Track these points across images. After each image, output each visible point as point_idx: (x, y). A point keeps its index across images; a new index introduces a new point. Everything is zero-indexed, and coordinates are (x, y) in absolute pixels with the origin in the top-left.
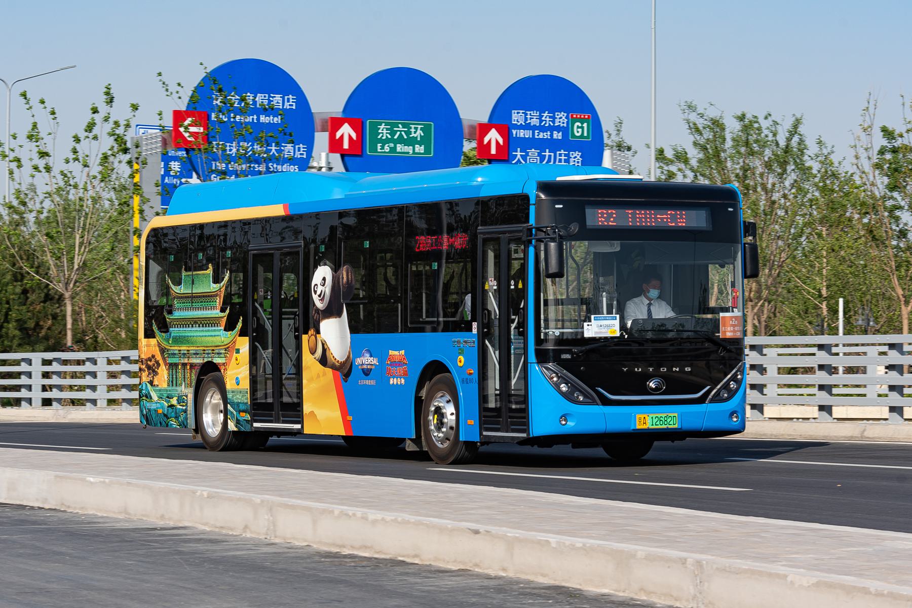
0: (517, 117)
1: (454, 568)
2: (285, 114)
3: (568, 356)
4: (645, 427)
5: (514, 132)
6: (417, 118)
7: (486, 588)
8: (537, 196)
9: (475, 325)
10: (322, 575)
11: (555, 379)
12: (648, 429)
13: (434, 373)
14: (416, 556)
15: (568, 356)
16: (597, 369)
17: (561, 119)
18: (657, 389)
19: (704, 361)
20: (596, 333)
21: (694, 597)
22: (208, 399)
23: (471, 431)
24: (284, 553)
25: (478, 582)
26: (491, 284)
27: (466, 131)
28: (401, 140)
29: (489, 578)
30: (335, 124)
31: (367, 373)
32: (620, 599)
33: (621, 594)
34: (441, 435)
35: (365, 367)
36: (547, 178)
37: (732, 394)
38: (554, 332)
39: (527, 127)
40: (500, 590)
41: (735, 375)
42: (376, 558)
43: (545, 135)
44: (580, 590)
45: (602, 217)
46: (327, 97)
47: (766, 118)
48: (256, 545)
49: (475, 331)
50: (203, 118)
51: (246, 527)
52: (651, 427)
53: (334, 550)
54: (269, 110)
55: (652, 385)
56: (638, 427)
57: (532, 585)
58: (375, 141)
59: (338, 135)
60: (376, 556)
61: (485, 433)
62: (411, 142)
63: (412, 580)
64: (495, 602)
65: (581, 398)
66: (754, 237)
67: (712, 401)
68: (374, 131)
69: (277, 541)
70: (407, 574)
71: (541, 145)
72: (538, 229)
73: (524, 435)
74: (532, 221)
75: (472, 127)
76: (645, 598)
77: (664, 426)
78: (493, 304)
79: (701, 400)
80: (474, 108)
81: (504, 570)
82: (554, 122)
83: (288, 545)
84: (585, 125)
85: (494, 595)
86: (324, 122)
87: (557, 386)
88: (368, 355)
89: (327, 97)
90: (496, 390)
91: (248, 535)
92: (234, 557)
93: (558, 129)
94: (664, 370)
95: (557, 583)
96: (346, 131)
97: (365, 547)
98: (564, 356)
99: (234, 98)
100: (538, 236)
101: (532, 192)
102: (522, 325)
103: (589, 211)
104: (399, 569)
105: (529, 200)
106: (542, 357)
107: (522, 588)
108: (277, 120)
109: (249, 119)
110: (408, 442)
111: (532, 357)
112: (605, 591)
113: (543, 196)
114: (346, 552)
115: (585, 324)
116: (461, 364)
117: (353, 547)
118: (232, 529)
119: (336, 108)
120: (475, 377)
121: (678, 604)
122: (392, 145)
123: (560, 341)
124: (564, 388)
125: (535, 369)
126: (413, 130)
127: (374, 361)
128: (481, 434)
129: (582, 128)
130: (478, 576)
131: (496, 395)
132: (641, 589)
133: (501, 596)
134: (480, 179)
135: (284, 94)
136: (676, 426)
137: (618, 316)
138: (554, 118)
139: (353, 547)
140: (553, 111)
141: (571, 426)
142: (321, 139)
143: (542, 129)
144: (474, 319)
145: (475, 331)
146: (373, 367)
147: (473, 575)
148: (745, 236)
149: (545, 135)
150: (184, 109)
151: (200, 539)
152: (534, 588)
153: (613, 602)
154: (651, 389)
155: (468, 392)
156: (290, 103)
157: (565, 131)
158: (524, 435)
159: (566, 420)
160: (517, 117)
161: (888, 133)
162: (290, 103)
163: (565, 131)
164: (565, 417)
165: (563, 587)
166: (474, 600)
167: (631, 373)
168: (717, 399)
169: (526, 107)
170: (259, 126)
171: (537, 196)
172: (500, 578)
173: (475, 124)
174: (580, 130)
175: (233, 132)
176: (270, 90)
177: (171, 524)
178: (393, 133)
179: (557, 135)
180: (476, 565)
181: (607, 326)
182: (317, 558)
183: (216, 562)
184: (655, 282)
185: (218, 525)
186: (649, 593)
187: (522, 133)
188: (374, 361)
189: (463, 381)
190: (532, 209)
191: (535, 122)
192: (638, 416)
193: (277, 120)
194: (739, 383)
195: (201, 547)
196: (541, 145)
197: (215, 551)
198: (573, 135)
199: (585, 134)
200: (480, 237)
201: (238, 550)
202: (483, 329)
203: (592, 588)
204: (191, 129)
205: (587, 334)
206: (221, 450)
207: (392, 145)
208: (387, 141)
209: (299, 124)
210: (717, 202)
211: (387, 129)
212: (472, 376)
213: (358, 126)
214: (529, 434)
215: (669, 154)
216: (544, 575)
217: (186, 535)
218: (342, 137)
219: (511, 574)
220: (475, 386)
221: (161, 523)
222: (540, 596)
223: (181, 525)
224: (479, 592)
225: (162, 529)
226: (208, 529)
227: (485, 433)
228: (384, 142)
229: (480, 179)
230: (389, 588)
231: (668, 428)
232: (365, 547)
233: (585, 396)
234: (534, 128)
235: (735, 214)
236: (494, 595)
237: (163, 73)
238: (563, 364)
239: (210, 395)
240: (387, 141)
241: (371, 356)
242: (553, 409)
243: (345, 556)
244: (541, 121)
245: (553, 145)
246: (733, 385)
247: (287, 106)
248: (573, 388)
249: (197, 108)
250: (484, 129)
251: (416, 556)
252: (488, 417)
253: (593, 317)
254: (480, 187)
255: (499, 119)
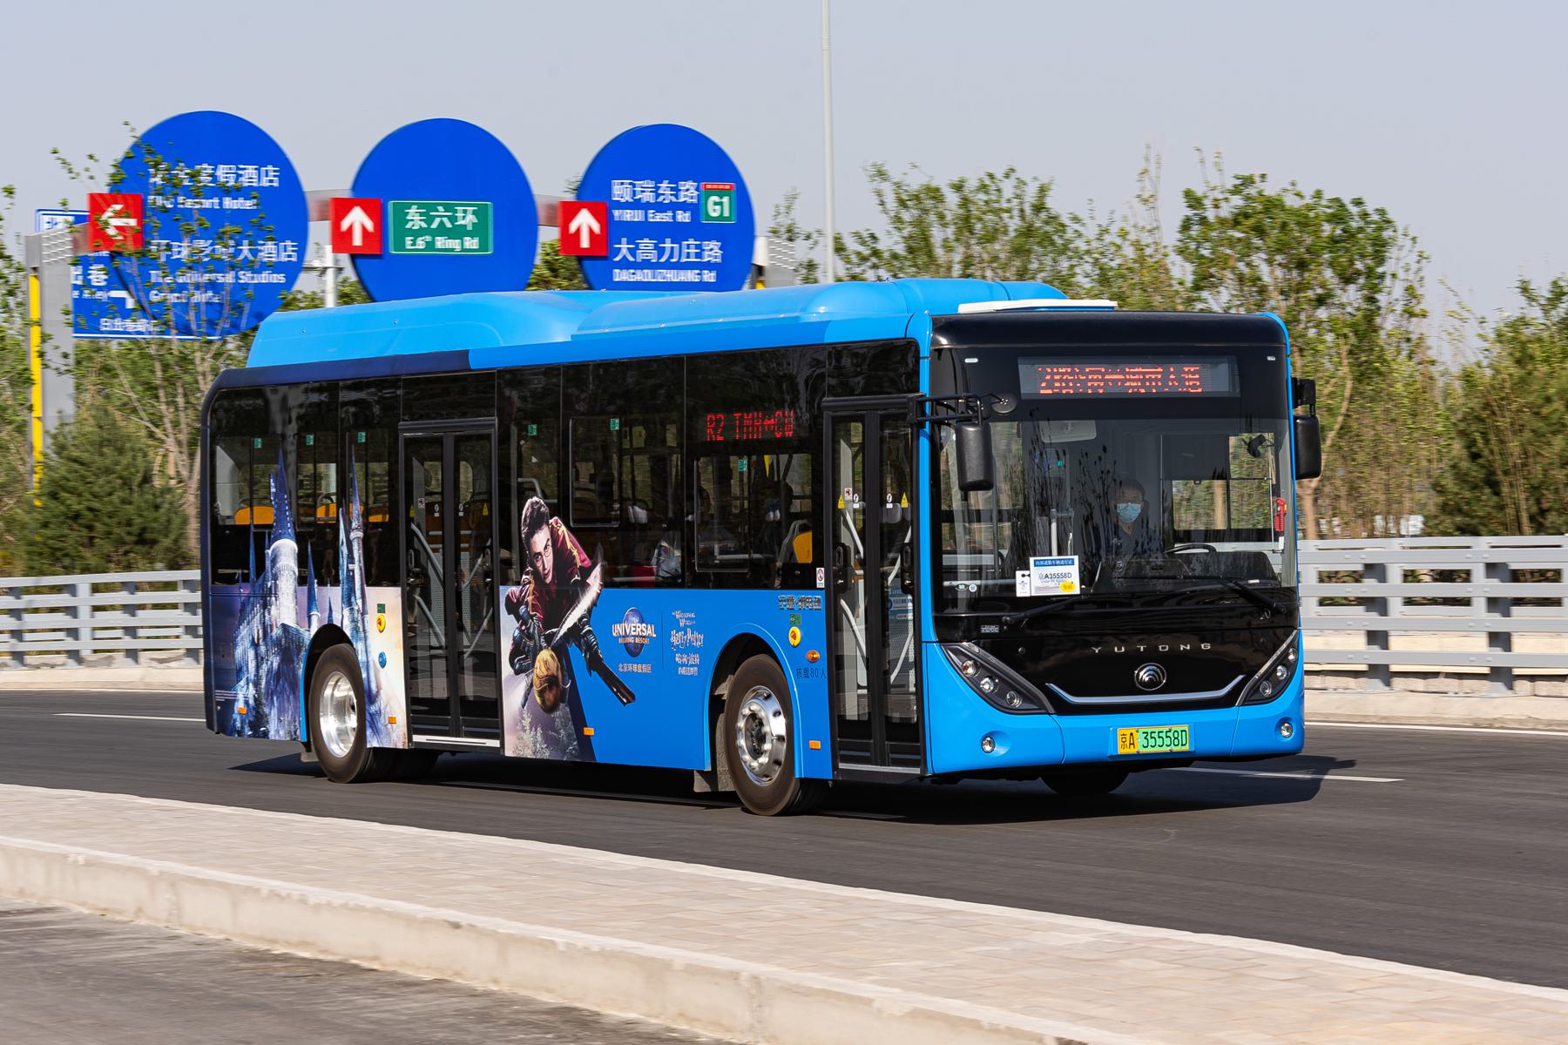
0: (620, 190)
1: (428, 977)
2: (262, 194)
3: (994, 629)
4: (1132, 751)
5: (616, 213)
6: (466, 195)
7: (461, 1013)
8: (934, 342)
9: (820, 572)
10: (234, 995)
11: (971, 671)
12: (1138, 754)
13: (743, 657)
14: (375, 958)
15: (994, 629)
16: (1043, 653)
17: (689, 191)
18: (1151, 683)
19: (1236, 628)
20: (1038, 589)
21: (751, 1028)
22: (328, 692)
23: (815, 758)
24: (190, 953)
25: (454, 1003)
26: (849, 497)
27: (542, 214)
28: (442, 231)
29: (474, 994)
30: (341, 207)
31: (634, 651)
32: (650, 1030)
33: (653, 1021)
34: (755, 764)
35: (631, 640)
36: (944, 311)
37: (1280, 688)
38: (967, 586)
39: (636, 205)
40: (483, 1017)
41: (1286, 653)
42: (320, 961)
43: (665, 217)
44: (598, 1014)
45: (1053, 379)
46: (327, 167)
47: (1007, 176)
48: (152, 940)
49: (821, 583)
50: (136, 206)
51: (139, 911)
52: (1143, 750)
53: (263, 947)
54: (237, 192)
55: (1144, 675)
56: (1121, 751)
57: (532, 1007)
58: (403, 232)
59: (345, 225)
60: (321, 957)
61: (842, 766)
62: (458, 232)
63: (361, 1000)
64: (470, 1038)
65: (1017, 702)
66: (1312, 404)
67: (1245, 703)
68: (402, 219)
69: (183, 931)
70: (356, 990)
71: (658, 232)
72: (937, 402)
73: (917, 771)
74: (925, 388)
75: (551, 207)
76: (685, 1027)
77: (1165, 749)
78: (851, 536)
79: (1227, 702)
80: (552, 175)
81: (496, 981)
82: (676, 196)
83: (197, 939)
84: (726, 200)
85: (471, 1026)
86: (323, 204)
87: (974, 684)
88: (635, 619)
89: (327, 167)
90: (859, 687)
91: (143, 922)
92: (115, 963)
93: (684, 206)
94: (1164, 648)
95: (567, 1003)
96: (358, 219)
97: (304, 944)
98: (986, 629)
99: (182, 173)
100: (943, 413)
101: (925, 336)
102: (910, 570)
103: (1025, 370)
104: (348, 981)
105: (917, 351)
106: (949, 630)
107: (517, 1012)
108: (248, 205)
109: (207, 204)
110: (697, 778)
111: (929, 632)
112: (632, 1016)
113: (944, 341)
114: (279, 950)
115: (1019, 574)
116: (796, 642)
117: (289, 944)
118: (119, 912)
119: (342, 185)
120: (823, 665)
121: (727, 1037)
122: (428, 238)
123: (975, 602)
124: (987, 684)
125: (935, 653)
126: (460, 215)
127: (649, 631)
128: (835, 767)
129: (721, 204)
130: (459, 991)
131: (859, 696)
132: (681, 1015)
133: (481, 1028)
134: (822, 309)
135: (260, 163)
136: (1186, 748)
137: (1076, 558)
138: (676, 190)
139: (289, 944)
140: (674, 180)
141: (1000, 753)
142: (319, 231)
143: (660, 207)
144: (819, 560)
145: (821, 583)
146: (646, 641)
147: (449, 990)
148: (1295, 406)
149: (665, 217)
150: (105, 190)
151: (70, 931)
152: (533, 1012)
153: (638, 1035)
154: (1143, 683)
155: (807, 689)
156: (269, 177)
157: (695, 209)
158: (917, 771)
159: (991, 743)
160: (620, 190)
161: (1193, 201)
162: (269, 177)
163: (695, 209)
164: (992, 737)
165: (575, 1009)
166: (441, 1035)
167: (1109, 657)
168: (1255, 698)
169: (634, 175)
170: (218, 215)
171: (934, 342)
172: (487, 994)
173: (556, 202)
174: (718, 208)
175: (176, 225)
176: (237, 158)
177: (34, 903)
178: (430, 220)
179: (683, 217)
180: (457, 974)
181: (1054, 576)
182: (234, 963)
183: (84, 973)
184: (1129, 493)
185: (103, 906)
186: (691, 1020)
187: (629, 215)
188: (649, 631)
189: (798, 673)
190: (925, 367)
191: (648, 197)
192: (1120, 731)
193: (248, 205)
194: (1291, 667)
195: (68, 944)
196: (658, 232)
197: (88, 952)
198: (709, 217)
199: (726, 214)
200: (827, 415)
201: (122, 949)
202: (836, 579)
203: (615, 1013)
204: (115, 221)
205: (1022, 591)
206: (352, 782)
207: (428, 238)
208: (421, 232)
209: (284, 209)
210: (1248, 344)
211: (421, 214)
212: (814, 666)
213: (376, 211)
214: (925, 768)
215: (852, 245)
216: (550, 991)
217: (52, 923)
218: (350, 229)
219: (504, 988)
220: (823, 683)
221: (19, 903)
222: (536, 1025)
223: (48, 905)
224: (451, 1020)
225: (21, 912)
226: (86, 911)
227: (842, 766)
228: (417, 234)
229: (822, 309)
230: (324, 1016)
231: (1171, 752)
232: (304, 944)
233: (1026, 696)
234: (646, 206)
235: (1278, 367)
236: (471, 1026)
237: (1269, 178)
238: (994, 645)
239: (332, 683)
240: (421, 232)
241: (642, 621)
242: (969, 721)
243: (277, 958)
244: (658, 195)
245: (677, 232)
246: (1281, 672)
247: (265, 183)
248: (1005, 684)
249: (128, 186)
250: (569, 210)
251: (375, 958)
252: (846, 735)
253: (1032, 560)
254: (824, 325)
255: (592, 192)
